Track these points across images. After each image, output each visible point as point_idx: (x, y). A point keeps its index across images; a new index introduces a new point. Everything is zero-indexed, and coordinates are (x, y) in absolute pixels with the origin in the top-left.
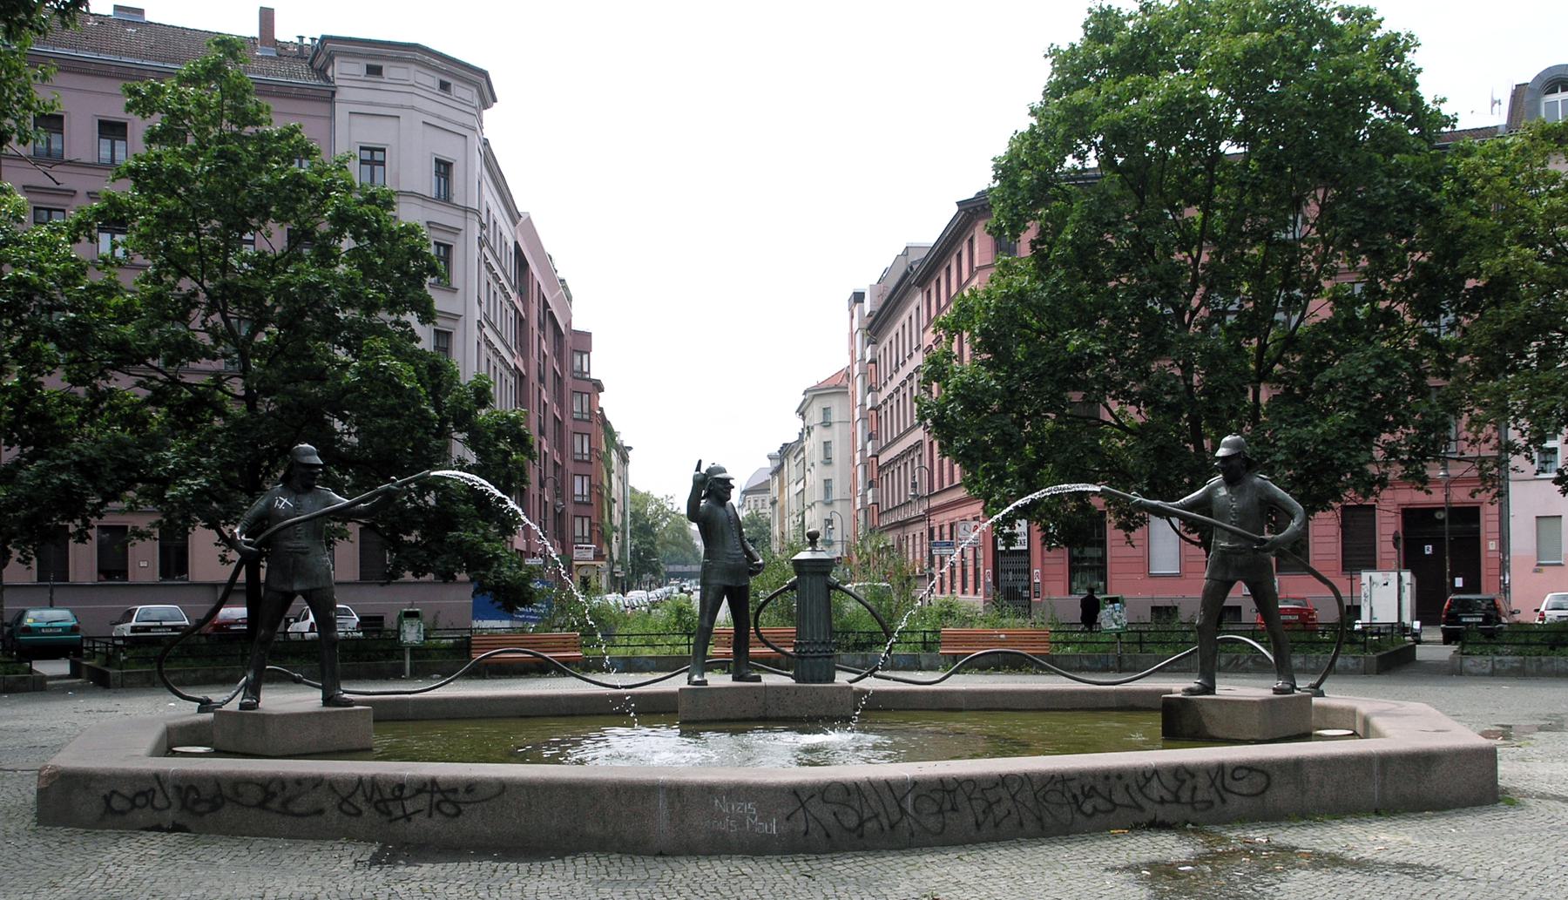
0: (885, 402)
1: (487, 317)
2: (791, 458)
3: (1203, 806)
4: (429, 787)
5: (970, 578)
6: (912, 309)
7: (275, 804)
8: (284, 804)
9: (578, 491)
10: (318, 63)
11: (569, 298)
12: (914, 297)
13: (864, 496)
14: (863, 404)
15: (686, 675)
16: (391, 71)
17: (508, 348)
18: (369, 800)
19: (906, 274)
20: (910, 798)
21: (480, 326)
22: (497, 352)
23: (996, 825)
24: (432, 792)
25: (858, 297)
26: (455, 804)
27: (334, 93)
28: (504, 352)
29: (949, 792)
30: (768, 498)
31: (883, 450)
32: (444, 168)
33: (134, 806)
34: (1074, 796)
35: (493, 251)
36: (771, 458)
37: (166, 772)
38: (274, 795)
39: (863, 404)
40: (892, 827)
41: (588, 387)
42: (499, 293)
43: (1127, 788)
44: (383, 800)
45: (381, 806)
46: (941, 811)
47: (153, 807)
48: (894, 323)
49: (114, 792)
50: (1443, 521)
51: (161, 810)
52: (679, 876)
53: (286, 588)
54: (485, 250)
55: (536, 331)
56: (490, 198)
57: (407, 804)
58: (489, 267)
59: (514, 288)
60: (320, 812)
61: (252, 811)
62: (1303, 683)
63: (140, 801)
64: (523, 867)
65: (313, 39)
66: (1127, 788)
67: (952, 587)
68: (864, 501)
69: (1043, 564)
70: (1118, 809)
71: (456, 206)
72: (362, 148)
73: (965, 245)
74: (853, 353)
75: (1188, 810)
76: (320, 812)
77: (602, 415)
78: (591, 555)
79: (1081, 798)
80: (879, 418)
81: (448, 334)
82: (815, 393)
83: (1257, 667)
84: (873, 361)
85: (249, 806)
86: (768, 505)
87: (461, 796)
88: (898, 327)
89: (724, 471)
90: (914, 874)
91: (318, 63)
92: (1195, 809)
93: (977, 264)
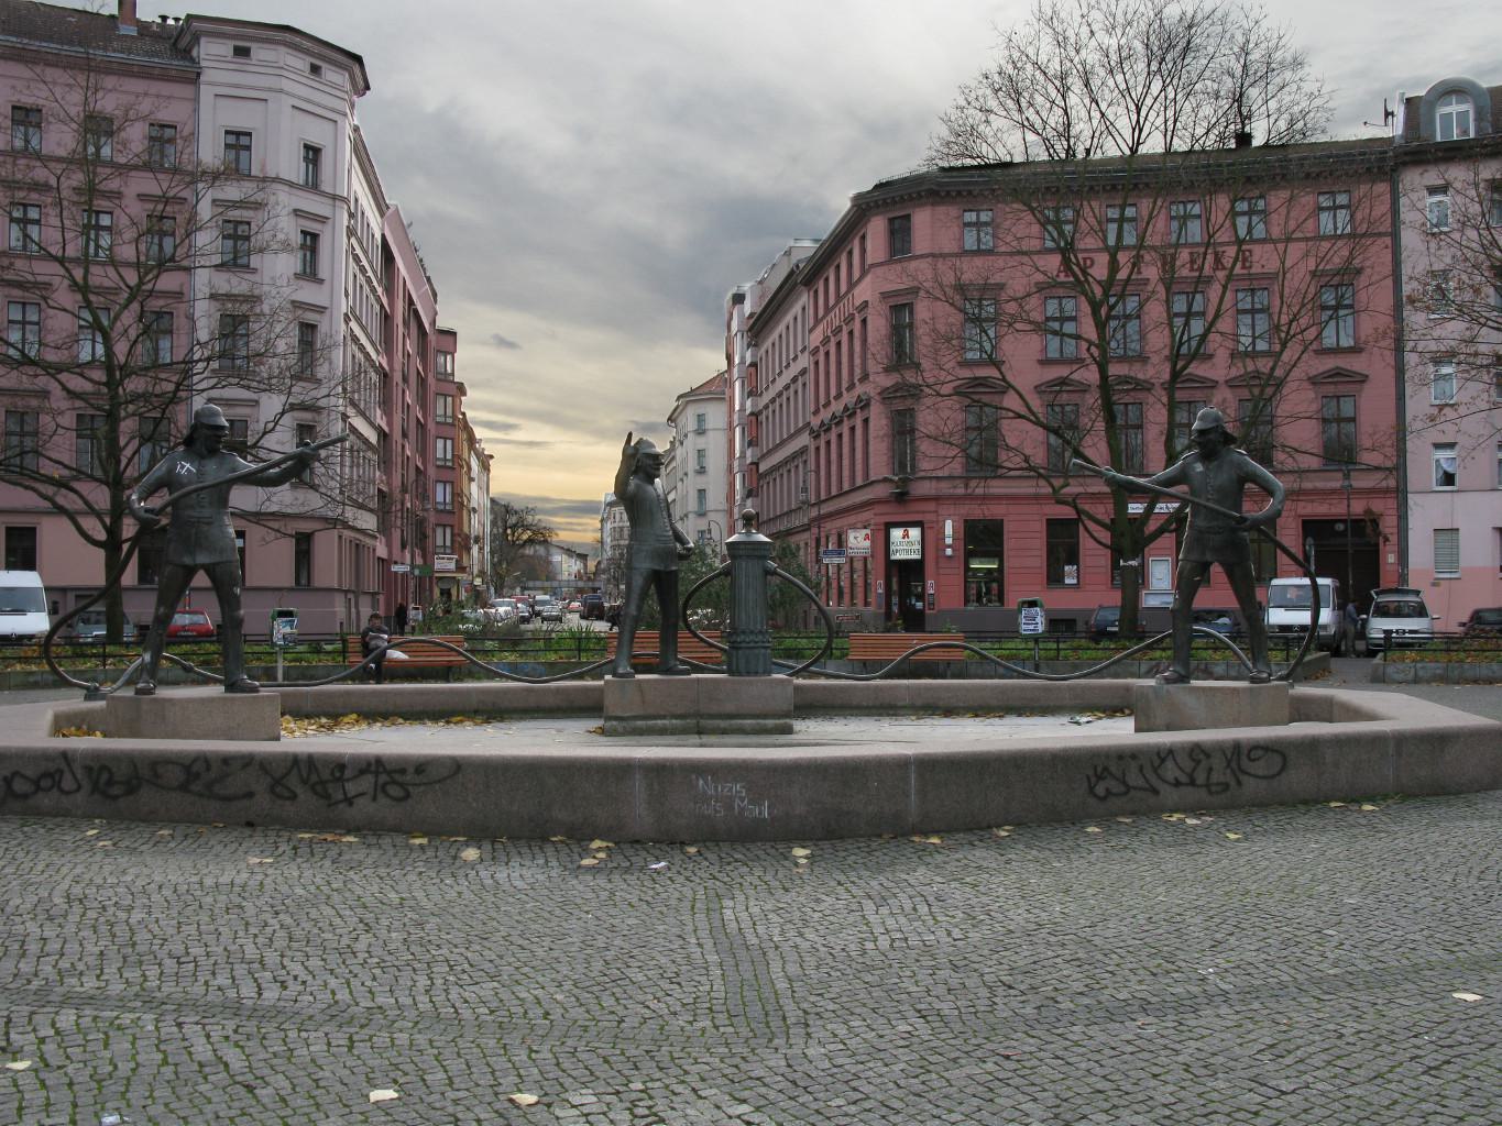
0: (766, 407)
1: (353, 311)
3: (1219, 788)
6: (797, 309)
10: (183, 44)
12: (800, 295)
16: (260, 53)
17: (372, 343)
18: (304, 782)
19: (792, 273)
21: (347, 319)
22: (362, 348)
24: (377, 774)
26: (401, 785)
27: (199, 74)
28: (369, 349)
31: (763, 457)
32: (313, 154)
33: (38, 788)
35: (360, 243)
37: (75, 751)
38: (197, 776)
39: (743, 409)
42: (366, 287)
43: (1141, 769)
44: (323, 783)
47: (62, 791)
48: (778, 323)
49: (16, 774)
51: (68, 793)
53: (187, 560)
54: (353, 240)
55: (401, 329)
56: (359, 187)
58: (357, 259)
59: (380, 282)
60: (250, 795)
63: (45, 783)
65: (177, 20)
66: (1141, 769)
67: (852, 598)
70: (1132, 792)
72: (227, 132)
73: (856, 242)
76: (250, 795)
78: (452, 566)
81: (313, 327)
84: (754, 365)
87: (408, 778)
88: (781, 328)
91: (183, 44)
92: (1210, 793)
93: (869, 261)
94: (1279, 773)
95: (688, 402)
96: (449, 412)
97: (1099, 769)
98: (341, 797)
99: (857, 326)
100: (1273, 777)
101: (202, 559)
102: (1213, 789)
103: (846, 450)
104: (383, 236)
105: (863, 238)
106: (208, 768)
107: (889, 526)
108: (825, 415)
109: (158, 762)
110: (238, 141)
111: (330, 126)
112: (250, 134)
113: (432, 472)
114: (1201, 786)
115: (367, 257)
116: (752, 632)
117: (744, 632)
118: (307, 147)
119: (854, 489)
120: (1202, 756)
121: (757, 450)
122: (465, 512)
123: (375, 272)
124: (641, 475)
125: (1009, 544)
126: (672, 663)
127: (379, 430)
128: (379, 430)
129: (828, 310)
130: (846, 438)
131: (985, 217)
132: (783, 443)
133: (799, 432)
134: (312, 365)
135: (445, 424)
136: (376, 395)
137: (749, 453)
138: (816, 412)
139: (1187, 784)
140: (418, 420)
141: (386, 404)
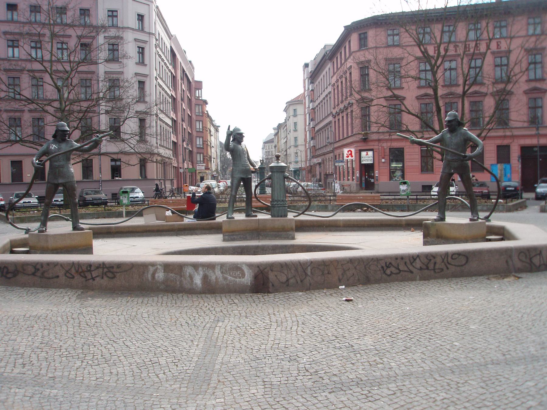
0: (317, 106)
1: (159, 75)
2: (282, 129)
3: (439, 271)
4: (102, 266)
5: (342, 175)
6: (327, 69)
7: (39, 274)
8: (43, 274)
9: (198, 143)
11: (193, 68)
12: (327, 65)
13: (310, 143)
14: (309, 107)
15: (226, 215)
17: (168, 87)
19: (324, 56)
20: (309, 269)
22: (163, 89)
23: (348, 280)
24: (103, 268)
25: (306, 65)
26: (113, 273)
29: (326, 266)
30: (273, 145)
31: (316, 125)
32: (141, 18)
34: (382, 267)
35: (161, 50)
36: (274, 129)
38: (38, 270)
39: (309, 107)
40: (301, 281)
41: (202, 103)
42: (164, 67)
43: (405, 263)
44: (83, 272)
45: (82, 274)
46: (323, 274)
50: (536, 152)
52: (206, 304)
53: (56, 182)
54: (158, 49)
56: (160, 29)
57: (93, 273)
59: (171, 64)
60: (58, 277)
61: (30, 277)
62: (482, 215)
64: (140, 300)
66: (405, 263)
68: (309, 145)
69: (379, 169)
70: (401, 273)
71: (146, 32)
72: (108, 11)
74: (304, 87)
75: (432, 272)
76: (58, 277)
77: (208, 114)
78: (203, 168)
79: (385, 268)
80: (315, 112)
82: (290, 104)
83: (462, 208)
84: (312, 90)
85: (28, 275)
86: (273, 148)
87: (115, 270)
88: (322, 76)
89: (239, 130)
90: (310, 303)
92: (435, 272)
93: (352, 50)
94: (465, 264)
95: (290, 105)
96: (201, 110)
97: (388, 264)
98: (90, 277)
99: (348, 74)
100: (462, 266)
101: (61, 181)
102: (437, 271)
103: (345, 122)
104: (171, 47)
105: (350, 42)
106: (42, 267)
107: (360, 151)
108: (337, 109)
109: (25, 265)
110: (113, 14)
111: (147, 6)
112: (117, 11)
113: (195, 134)
114: (431, 270)
115: (164, 55)
116: (279, 201)
117: (276, 201)
118: (139, 15)
119: (348, 137)
120: (432, 258)
121: (314, 122)
122: (209, 148)
123: (168, 61)
124: (236, 141)
125: (406, 157)
126: (250, 213)
127: (172, 119)
128: (172, 119)
129: (338, 69)
130: (345, 118)
131: (396, 32)
132: (323, 119)
133: (328, 115)
134: (144, 96)
135: (199, 115)
136: (170, 107)
137: (311, 123)
138: (334, 108)
139: (425, 269)
140: (188, 114)
141: (175, 110)
